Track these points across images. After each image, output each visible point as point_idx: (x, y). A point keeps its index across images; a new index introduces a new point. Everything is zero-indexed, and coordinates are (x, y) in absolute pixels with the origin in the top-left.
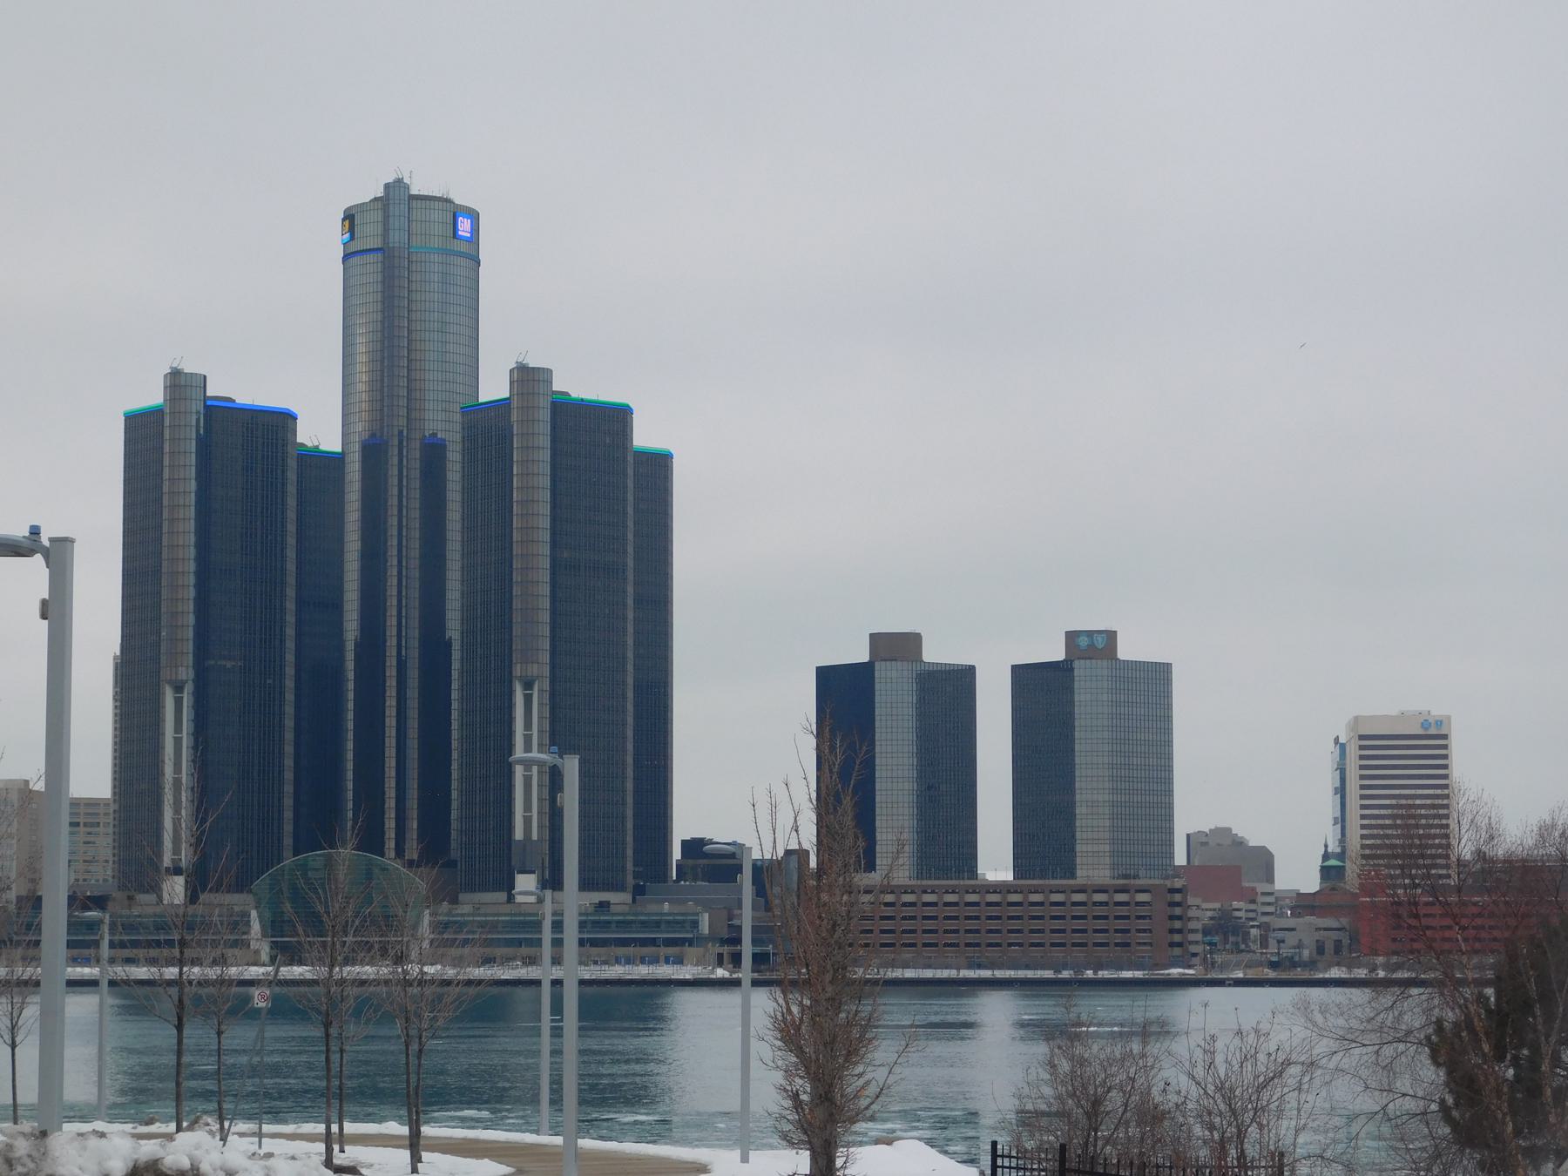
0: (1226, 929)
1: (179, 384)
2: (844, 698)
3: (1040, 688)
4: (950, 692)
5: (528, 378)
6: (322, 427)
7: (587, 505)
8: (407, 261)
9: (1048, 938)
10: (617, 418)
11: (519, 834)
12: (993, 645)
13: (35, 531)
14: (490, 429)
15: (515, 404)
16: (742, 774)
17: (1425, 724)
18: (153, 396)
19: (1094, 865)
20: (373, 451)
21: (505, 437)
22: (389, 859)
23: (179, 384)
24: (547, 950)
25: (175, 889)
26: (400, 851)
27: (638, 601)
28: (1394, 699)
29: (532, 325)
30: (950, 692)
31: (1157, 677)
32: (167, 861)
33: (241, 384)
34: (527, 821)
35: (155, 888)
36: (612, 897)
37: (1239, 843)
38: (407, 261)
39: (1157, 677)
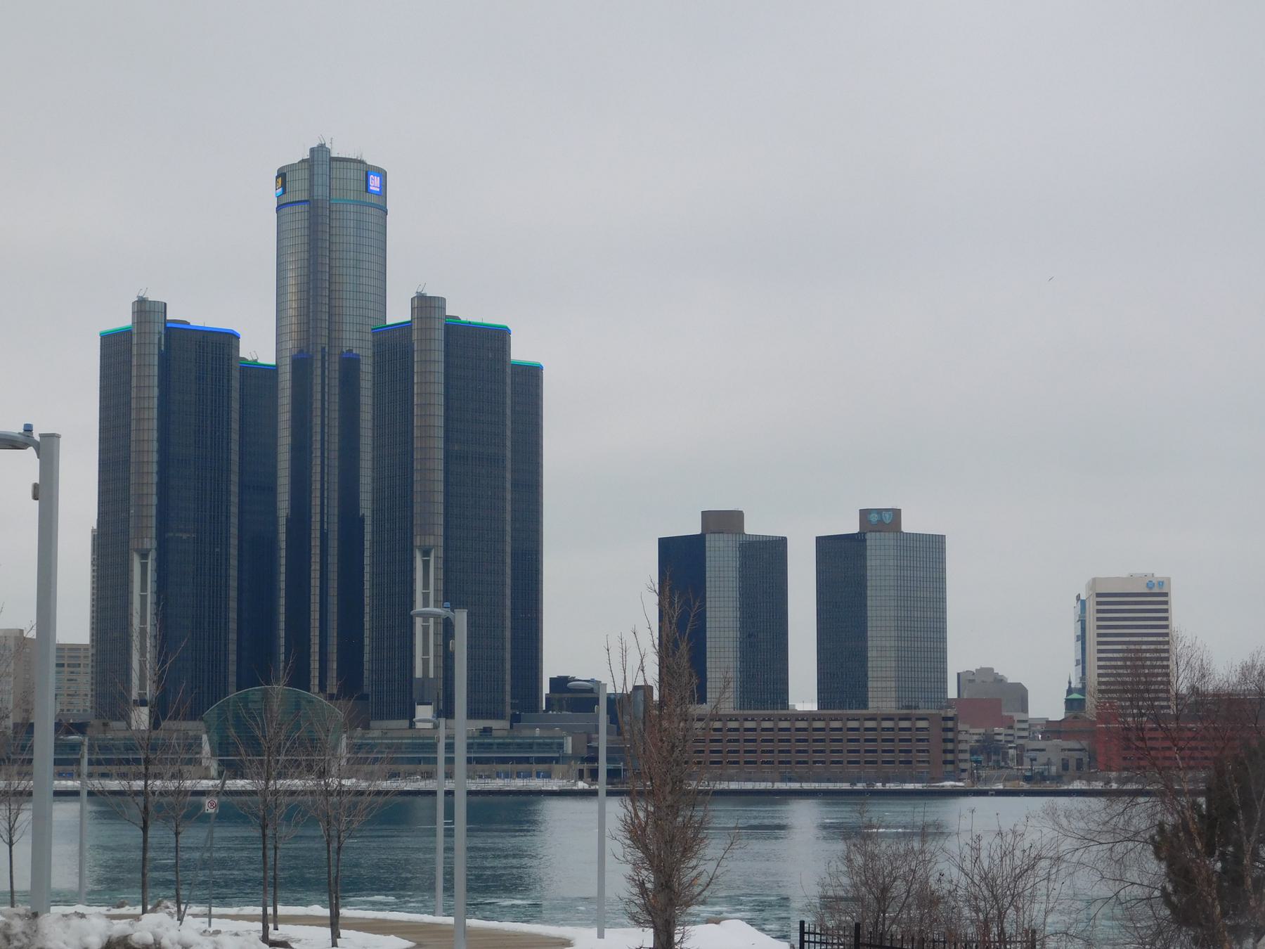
0: (989, 750)
1: (145, 310)
2: (681, 563)
3: (839, 555)
4: (767, 558)
5: (426, 305)
6: (259, 345)
7: (473, 407)
8: (328, 211)
9: (846, 757)
10: (498, 337)
11: (418, 673)
12: (801, 520)
13: (28, 429)
14: (395, 346)
15: (415, 326)
16: (599, 625)
17: (1150, 585)
18: (123, 320)
19: (882, 698)
20: (301, 364)
21: (407, 352)
22: (314, 693)
23: (145, 310)
24: (441, 766)
25: (141, 718)
26: (322, 687)
27: (515, 485)
28: (1124, 564)
29: (429, 262)
30: (767, 558)
31: (933, 547)
32: (135, 694)
33: (194, 310)
34: (425, 663)
35: (125, 717)
36: (494, 724)
37: (1000, 680)
38: (328, 211)
39: (933, 547)
